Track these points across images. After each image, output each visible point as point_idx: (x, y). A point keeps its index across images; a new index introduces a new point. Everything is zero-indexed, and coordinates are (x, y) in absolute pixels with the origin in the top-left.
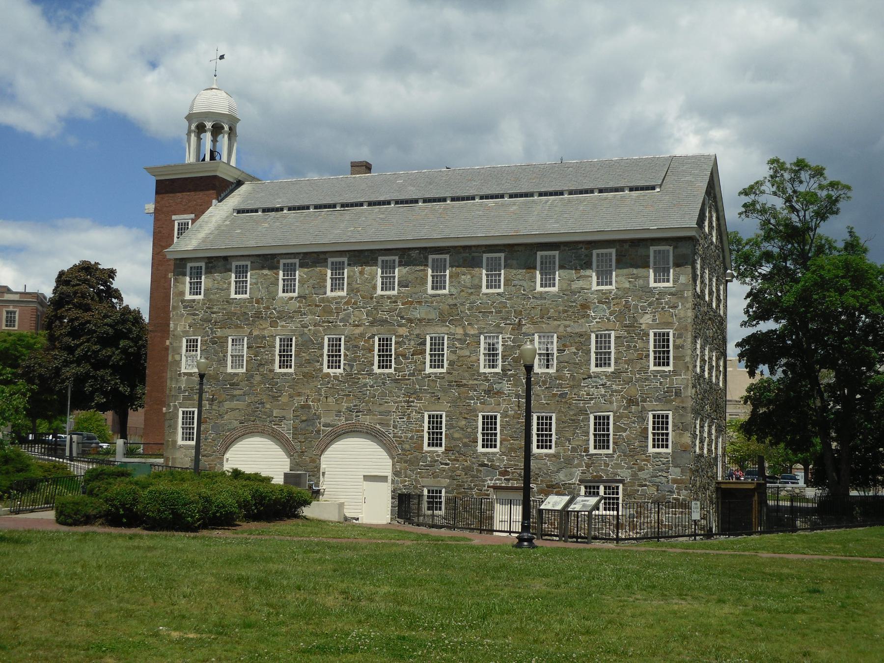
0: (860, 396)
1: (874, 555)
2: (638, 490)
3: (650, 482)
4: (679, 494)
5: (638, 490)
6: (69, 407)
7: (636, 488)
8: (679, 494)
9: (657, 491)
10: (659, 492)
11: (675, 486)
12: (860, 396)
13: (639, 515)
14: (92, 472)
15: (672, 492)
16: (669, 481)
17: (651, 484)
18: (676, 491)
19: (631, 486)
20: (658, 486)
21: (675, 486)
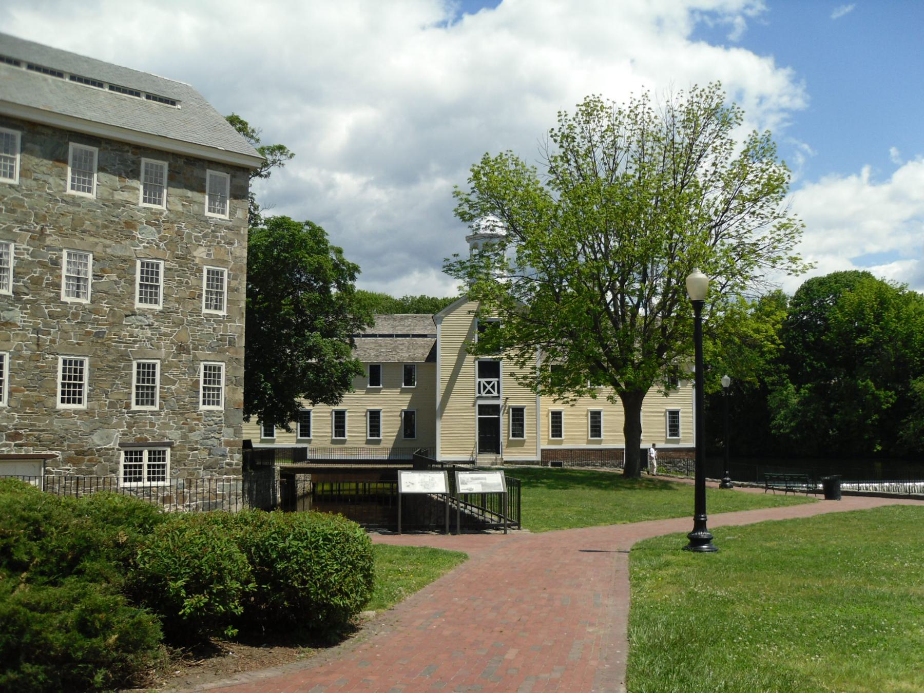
2: (189, 455)
3: (201, 444)
7: (187, 452)
9: (209, 455)
11: (228, 449)
15: (224, 456)
18: (229, 455)
19: (181, 450)
20: (210, 449)
21: (228, 449)
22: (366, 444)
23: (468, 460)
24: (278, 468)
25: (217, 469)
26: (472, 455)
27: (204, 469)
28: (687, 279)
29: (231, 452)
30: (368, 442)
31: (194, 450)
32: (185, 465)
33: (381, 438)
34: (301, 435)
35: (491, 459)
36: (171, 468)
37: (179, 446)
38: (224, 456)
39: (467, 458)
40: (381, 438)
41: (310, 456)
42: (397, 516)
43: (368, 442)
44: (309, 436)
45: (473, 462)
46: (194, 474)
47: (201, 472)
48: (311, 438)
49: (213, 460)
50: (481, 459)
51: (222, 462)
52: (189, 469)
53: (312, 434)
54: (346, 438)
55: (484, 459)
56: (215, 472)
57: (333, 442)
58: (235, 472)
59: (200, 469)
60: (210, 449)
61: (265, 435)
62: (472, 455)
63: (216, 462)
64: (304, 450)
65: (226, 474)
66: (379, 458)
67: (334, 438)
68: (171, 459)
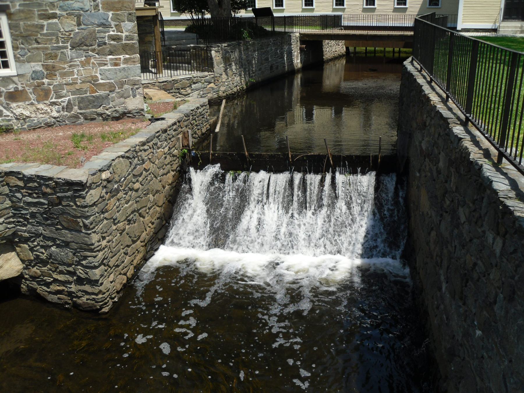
0: (188, 345)
1: (468, 66)
2: (42, 27)
3: (61, 8)
4: (119, 28)
5: (42, 27)
6: (244, 144)
7: (37, 21)
8: (119, 28)
9: (79, 24)
10: (83, 26)
11: (110, 14)
12: (188, 345)
13: (51, 71)
14: (135, 147)
15: (105, 25)
16: (97, 5)
17: (64, 13)
18: (113, 24)
19: (26, 19)
20: (79, 16)
21: (110, 14)
22: (393, 12)
23: (490, 27)
24: (298, 35)
25: (95, 47)
26: (495, 23)
27: (73, 48)
28: (137, 174)
29: (116, 18)
30: (395, 10)
31: (49, 18)
32: (38, 43)
33: (407, 6)
34: (336, 5)
35: (516, 27)
36: (15, 48)
37: (20, 11)
38: (105, 25)
39: (489, 26)
40: (407, 6)
41: (345, 23)
42: (435, 26)
43: (395, 10)
44: (343, 5)
45: (495, 30)
46: (56, 56)
47: (69, 52)
48: (345, 6)
49: (85, 33)
50: (504, 27)
51: (102, 35)
52: (47, 48)
53: (345, 3)
54: (376, 6)
55: (508, 27)
56: (93, 50)
57: (364, 10)
58: (126, 49)
59: (66, 48)
60: (79, 16)
61: (306, 5)
62: (495, 23)
63: (92, 36)
64: (339, 18)
65: (111, 53)
66: (398, 25)
67: (365, 6)
68: (12, 35)
